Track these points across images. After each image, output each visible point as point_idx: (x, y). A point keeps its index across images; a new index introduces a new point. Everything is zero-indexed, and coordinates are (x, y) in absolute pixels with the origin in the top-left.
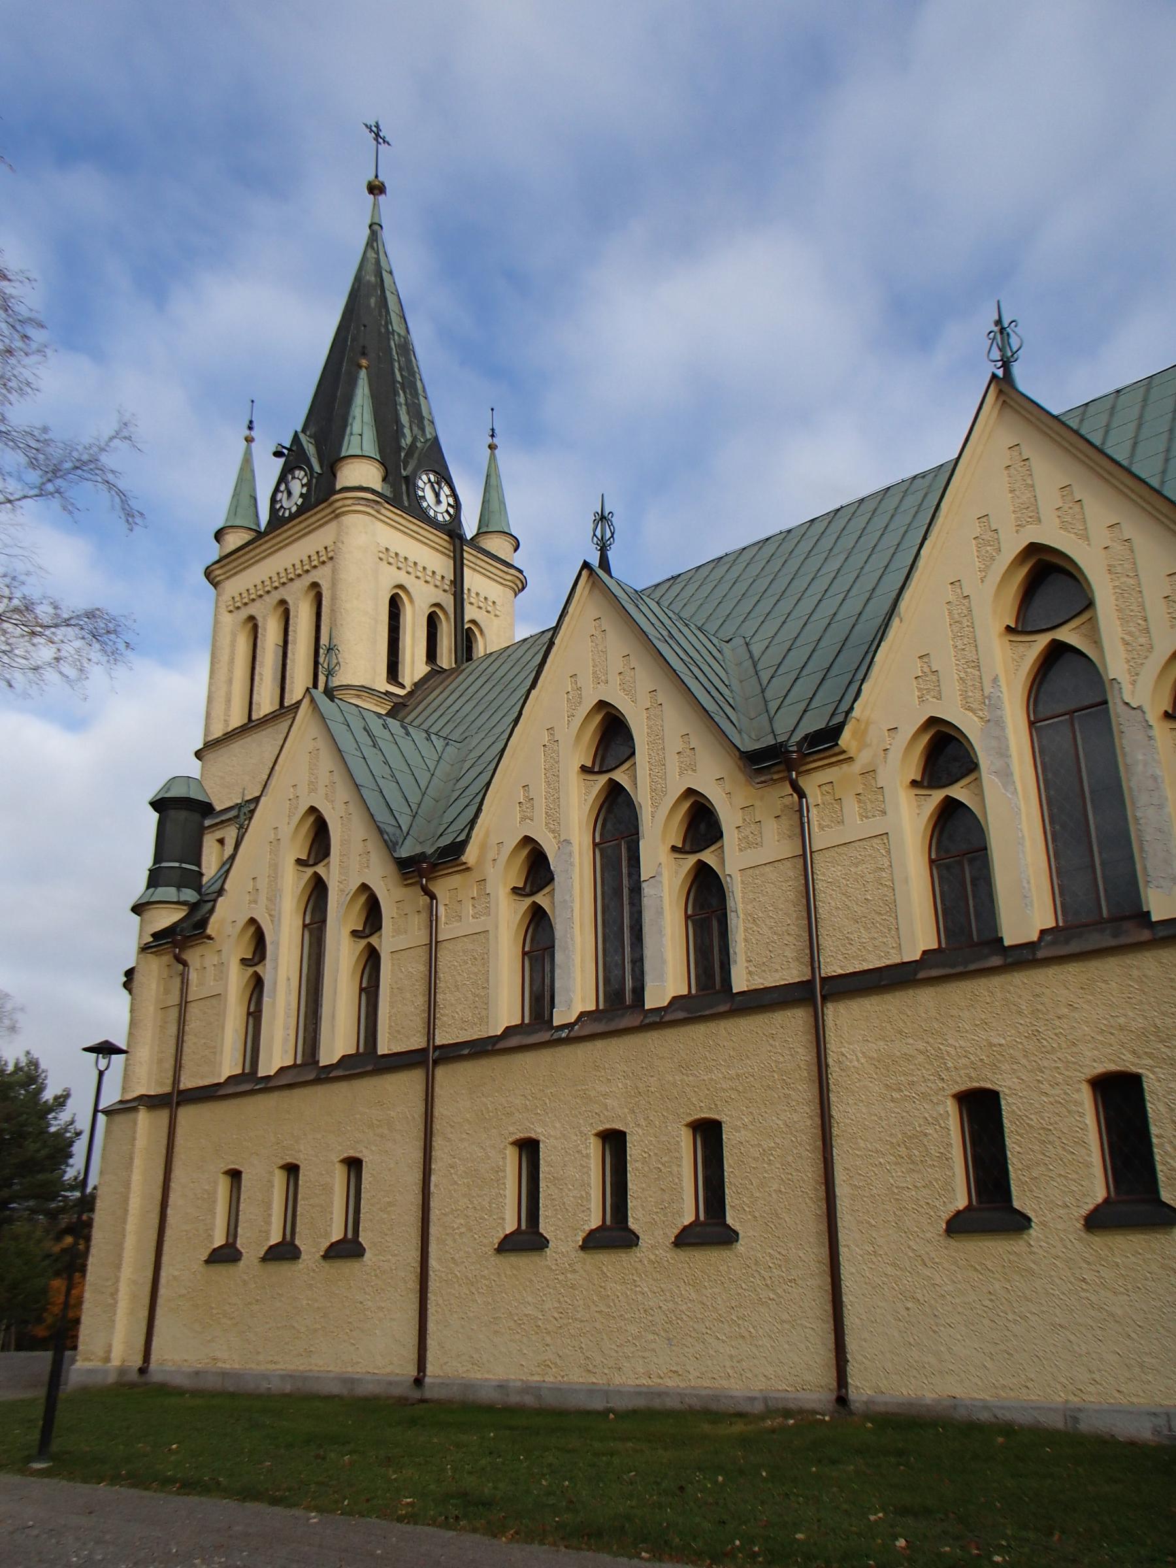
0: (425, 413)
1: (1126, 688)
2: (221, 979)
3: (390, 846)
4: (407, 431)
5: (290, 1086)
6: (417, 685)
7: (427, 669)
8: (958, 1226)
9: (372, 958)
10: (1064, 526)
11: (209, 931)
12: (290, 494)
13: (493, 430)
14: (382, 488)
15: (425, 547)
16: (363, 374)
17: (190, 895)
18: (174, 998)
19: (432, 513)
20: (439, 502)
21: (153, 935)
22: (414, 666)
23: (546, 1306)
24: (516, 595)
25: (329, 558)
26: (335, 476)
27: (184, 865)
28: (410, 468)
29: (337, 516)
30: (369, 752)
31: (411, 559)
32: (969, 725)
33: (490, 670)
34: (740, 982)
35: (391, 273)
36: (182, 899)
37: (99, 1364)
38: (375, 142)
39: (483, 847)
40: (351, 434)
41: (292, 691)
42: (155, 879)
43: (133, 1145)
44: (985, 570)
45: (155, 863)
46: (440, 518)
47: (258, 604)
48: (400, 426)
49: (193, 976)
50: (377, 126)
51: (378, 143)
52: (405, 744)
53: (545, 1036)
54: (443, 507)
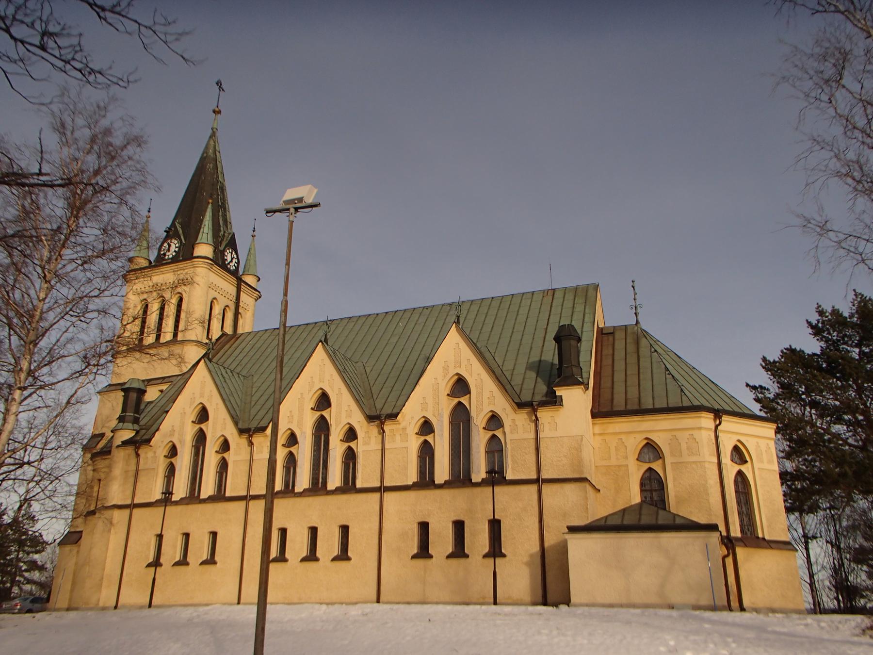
2: (155, 463)
3: (236, 423)
4: (222, 228)
6: (217, 340)
7: (220, 333)
10: (466, 370)
11: (151, 444)
15: (226, 282)
16: (210, 206)
17: (136, 427)
18: (133, 467)
21: (122, 442)
24: (256, 301)
26: (193, 249)
31: (217, 285)
33: (258, 345)
35: (219, 152)
40: (203, 232)
42: (121, 419)
44: (444, 377)
46: (232, 268)
48: (220, 226)
49: (142, 461)
51: (220, 90)
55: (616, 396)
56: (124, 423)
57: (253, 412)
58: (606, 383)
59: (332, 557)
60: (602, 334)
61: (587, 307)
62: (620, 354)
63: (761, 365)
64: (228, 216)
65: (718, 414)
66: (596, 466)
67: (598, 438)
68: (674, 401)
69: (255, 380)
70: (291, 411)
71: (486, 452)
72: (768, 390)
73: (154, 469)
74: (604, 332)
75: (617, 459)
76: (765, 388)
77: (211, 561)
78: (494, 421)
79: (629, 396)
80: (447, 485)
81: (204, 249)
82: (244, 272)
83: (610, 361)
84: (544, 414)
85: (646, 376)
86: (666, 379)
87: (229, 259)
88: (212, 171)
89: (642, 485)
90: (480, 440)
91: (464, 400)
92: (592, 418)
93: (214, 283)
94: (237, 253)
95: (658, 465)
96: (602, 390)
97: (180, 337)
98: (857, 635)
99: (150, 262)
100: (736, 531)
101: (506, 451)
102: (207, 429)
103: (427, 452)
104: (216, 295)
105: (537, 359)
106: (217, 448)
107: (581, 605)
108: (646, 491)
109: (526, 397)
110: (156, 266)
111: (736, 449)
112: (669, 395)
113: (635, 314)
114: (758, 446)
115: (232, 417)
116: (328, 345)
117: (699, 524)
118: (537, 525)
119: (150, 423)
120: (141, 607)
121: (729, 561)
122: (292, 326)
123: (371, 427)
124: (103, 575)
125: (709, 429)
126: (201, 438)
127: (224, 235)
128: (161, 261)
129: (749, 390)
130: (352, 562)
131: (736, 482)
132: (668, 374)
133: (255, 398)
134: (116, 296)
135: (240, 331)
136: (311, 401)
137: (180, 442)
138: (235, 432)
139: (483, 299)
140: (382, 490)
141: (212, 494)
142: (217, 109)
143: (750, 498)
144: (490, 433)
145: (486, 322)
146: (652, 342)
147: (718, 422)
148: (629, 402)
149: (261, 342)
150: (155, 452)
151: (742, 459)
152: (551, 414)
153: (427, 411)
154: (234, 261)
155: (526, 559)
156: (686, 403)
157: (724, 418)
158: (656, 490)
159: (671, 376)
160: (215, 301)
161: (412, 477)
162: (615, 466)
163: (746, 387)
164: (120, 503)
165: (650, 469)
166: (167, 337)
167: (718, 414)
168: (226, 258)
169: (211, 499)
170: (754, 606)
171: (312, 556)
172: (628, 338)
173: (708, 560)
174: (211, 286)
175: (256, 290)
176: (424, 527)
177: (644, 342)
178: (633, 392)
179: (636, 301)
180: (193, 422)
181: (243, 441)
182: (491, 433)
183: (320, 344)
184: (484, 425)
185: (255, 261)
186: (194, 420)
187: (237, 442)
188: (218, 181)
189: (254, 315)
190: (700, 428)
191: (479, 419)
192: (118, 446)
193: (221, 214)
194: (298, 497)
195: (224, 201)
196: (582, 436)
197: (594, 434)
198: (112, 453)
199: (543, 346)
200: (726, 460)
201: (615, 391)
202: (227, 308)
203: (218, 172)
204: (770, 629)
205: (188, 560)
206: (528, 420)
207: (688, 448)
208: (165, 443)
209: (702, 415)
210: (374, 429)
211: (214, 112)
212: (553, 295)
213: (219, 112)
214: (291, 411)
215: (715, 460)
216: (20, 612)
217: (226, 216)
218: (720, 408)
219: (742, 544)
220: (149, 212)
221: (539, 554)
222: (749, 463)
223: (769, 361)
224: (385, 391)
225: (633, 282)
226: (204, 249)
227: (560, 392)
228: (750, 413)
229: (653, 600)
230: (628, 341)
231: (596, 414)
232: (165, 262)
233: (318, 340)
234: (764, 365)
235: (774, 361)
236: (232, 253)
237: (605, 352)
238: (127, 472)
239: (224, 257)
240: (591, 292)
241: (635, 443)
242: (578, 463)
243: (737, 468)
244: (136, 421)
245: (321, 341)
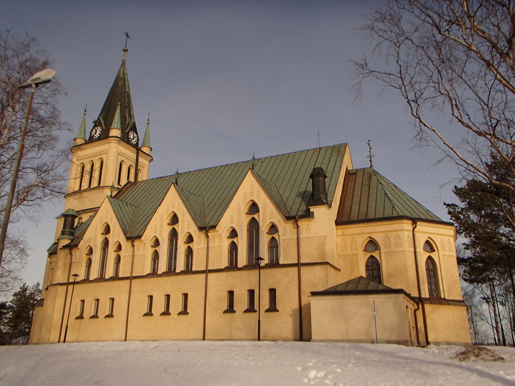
0: (132, 114)
1: (262, 228)
3: (125, 234)
4: (127, 119)
6: (125, 186)
7: (127, 182)
8: (225, 312)
9: (118, 258)
11: (78, 247)
14: (121, 136)
16: (119, 106)
17: (71, 237)
18: (69, 261)
21: (63, 246)
24: (150, 162)
25: (106, 152)
27: (71, 230)
29: (109, 143)
30: (120, 211)
32: (237, 230)
33: (147, 188)
34: (194, 269)
35: (127, 74)
38: (126, 38)
39: (146, 237)
40: (115, 122)
42: (63, 233)
44: (244, 202)
46: (134, 143)
47: (85, 160)
48: (126, 118)
50: (128, 34)
51: (127, 37)
55: (352, 212)
56: (64, 235)
57: (137, 227)
58: (348, 203)
59: (178, 313)
60: (349, 174)
61: (339, 157)
62: (358, 186)
63: (453, 191)
64: (132, 112)
65: (414, 221)
66: (338, 255)
67: (340, 238)
68: (388, 214)
69: (141, 208)
70: (156, 226)
71: (268, 247)
72: (457, 206)
73: (80, 262)
74: (351, 172)
75: (352, 250)
76: (455, 205)
77: (110, 316)
78: (273, 228)
79: (361, 211)
80: (245, 268)
81: (115, 132)
82: (142, 145)
83: (351, 191)
84: (302, 223)
85: (372, 199)
86: (384, 200)
87: (132, 137)
88: (122, 86)
89: (367, 266)
90: (264, 240)
91: (255, 216)
92: (336, 225)
93: (124, 153)
94: (137, 134)
95: (376, 254)
96: (345, 208)
97: (101, 185)
98: (452, 358)
99: (86, 141)
100: (425, 294)
101: (280, 246)
102: (109, 237)
103: (233, 248)
104: (123, 159)
105: (304, 190)
106: (115, 249)
107: (318, 341)
108: (370, 270)
109: (293, 214)
110: (88, 143)
111: (427, 242)
112: (386, 209)
113: (370, 161)
114: (442, 240)
115: (123, 231)
116: (178, 185)
117: (392, 289)
118: (297, 291)
119: (80, 235)
121: (419, 313)
122: (167, 176)
123: (201, 234)
124: (52, 324)
125: (410, 230)
127: (129, 124)
128: (91, 140)
129: (446, 207)
130: (189, 315)
131: (427, 263)
132: (387, 197)
133: (139, 219)
134: (35, 158)
135: (139, 179)
136: (167, 220)
137: (95, 245)
138: (124, 238)
139: (278, 156)
140: (207, 272)
141: (112, 276)
142: (125, 49)
143: (437, 273)
144: (271, 236)
145: (277, 169)
146: (379, 178)
147: (414, 226)
148: (360, 215)
149: (148, 186)
150: (81, 252)
151: (432, 249)
152: (307, 223)
153: (233, 223)
154: (135, 139)
155: (290, 312)
156: (395, 214)
157: (419, 223)
158: (375, 270)
159: (388, 198)
161: (225, 263)
162: (350, 255)
163: (444, 205)
164: (61, 282)
165: (372, 256)
166: (95, 184)
167: (414, 221)
168: (130, 137)
170: (437, 341)
171: (166, 313)
172: (365, 176)
173: (375, 311)
174: (120, 154)
175: (149, 156)
176: (231, 293)
177: (374, 178)
178: (363, 209)
179: (371, 153)
180: (102, 234)
181: (129, 244)
182: (271, 236)
183: (173, 185)
184: (267, 231)
185: (149, 139)
186: (103, 233)
187: (126, 245)
188: (125, 92)
189: (148, 170)
190: (403, 230)
191: (264, 228)
192: (61, 249)
193: (127, 111)
194: (159, 277)
195: (130, 103)
196: (325, 236)
197: (337, 236)
198: (57, 252)
199: (308, 182)
200: (420, 249)
201: (353, 208)
202: (131, 167)
203: (125, 86)
204: (398, 354)
205: (98, 315)
206: (293, 227)
207: (395, 243)
208: (86, 246)
209: (404, 222)
210: (203, 235)
211: (124, 50)
212: (320, 151)
213: (127, 50)
214: (156, 226)
215: (413, 250)
216: (22, 344)
217: (131, 112)
218: (404, 215)
219: (429, 302)
220: (85, 111)
221: (299, 310)
222: (436, 252)
223: (458, 188)
224: (212, 213)
225: (369, 141)
226: (115, 132)
227: (313, 209)
228: (438, 220)
229: (362, 337)
230: (364, 178)
231: (338, 223)
232: (93, 140)
234: (455, 191)
235: (461, 188)
236: (134, 134)
237: (349, 185)
238: (65, 264)
239: (128, 136)
240: (342, 149)
241: (362, 240)
242: (323, 253)
243: (428, 255)
244: (71, 234)
245: (173, 183)
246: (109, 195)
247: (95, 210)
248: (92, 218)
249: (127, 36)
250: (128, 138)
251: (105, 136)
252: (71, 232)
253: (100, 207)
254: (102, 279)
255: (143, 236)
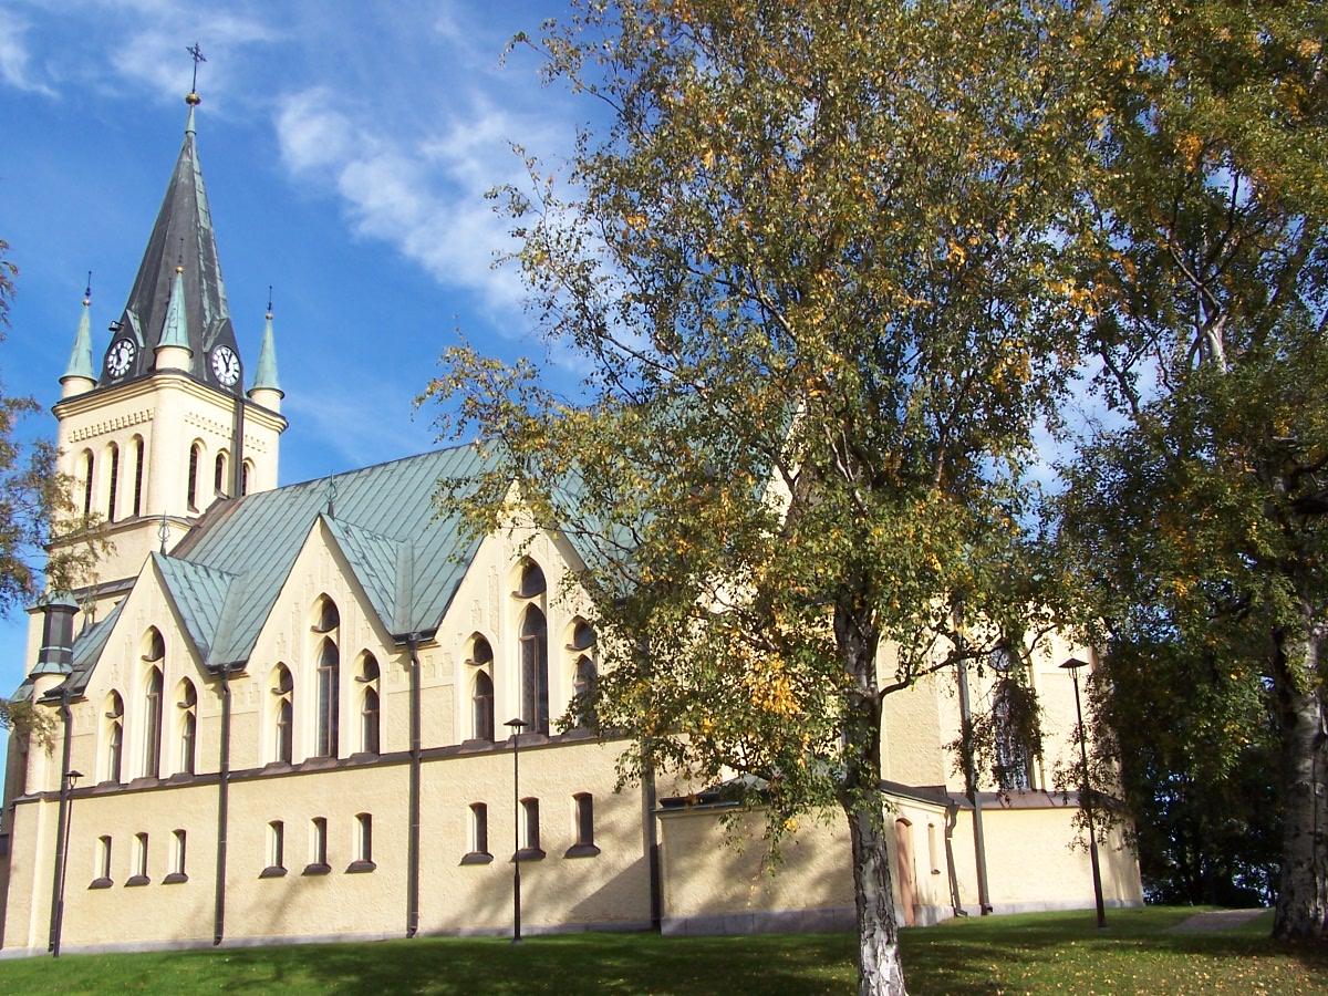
4: (207, 313)
5: (141, 790)
7: (216, 498)
9: (191, 721)
12: (119, 360)
13: (270, 304)
16: (179, 278)
17: (67, 668)
19: (222, 379)
20: (228, 370)
22: (205, 497)
23: (688, 122)
27: (64, 649)
28: (209, 345)
29: (157, 389)
30: (188, 593)
33: (267, 517)
36: (63, 671)
37: (20, 947)
41: (120, 511)
42: (43, 657)
43: (37, 822)
45: (43, 646)
50: (197, 49)
52: (207, 582)
53: (288, 770)
54: (231, 372)
81: (174, 358)
97: (142, 513)
116: (333, 519)
120: (641, 931)
126: (331, 653)
135: (251, 489)
142: (194, 96)
160: (199, 443)
161: (466, 730)
168: (215, 365)
169: (358, 762)
232: (114, 382)
233: (316, 513)
244: (66, 658)
246: (157, 550)
247: (123, 588)
248: (120, 607)
249: (196, 54)
250: (211, 370)
251: (145, 373)
252: (64, 653)
253: (137, 578)
254: (153, 782)
255: (250, 661)
